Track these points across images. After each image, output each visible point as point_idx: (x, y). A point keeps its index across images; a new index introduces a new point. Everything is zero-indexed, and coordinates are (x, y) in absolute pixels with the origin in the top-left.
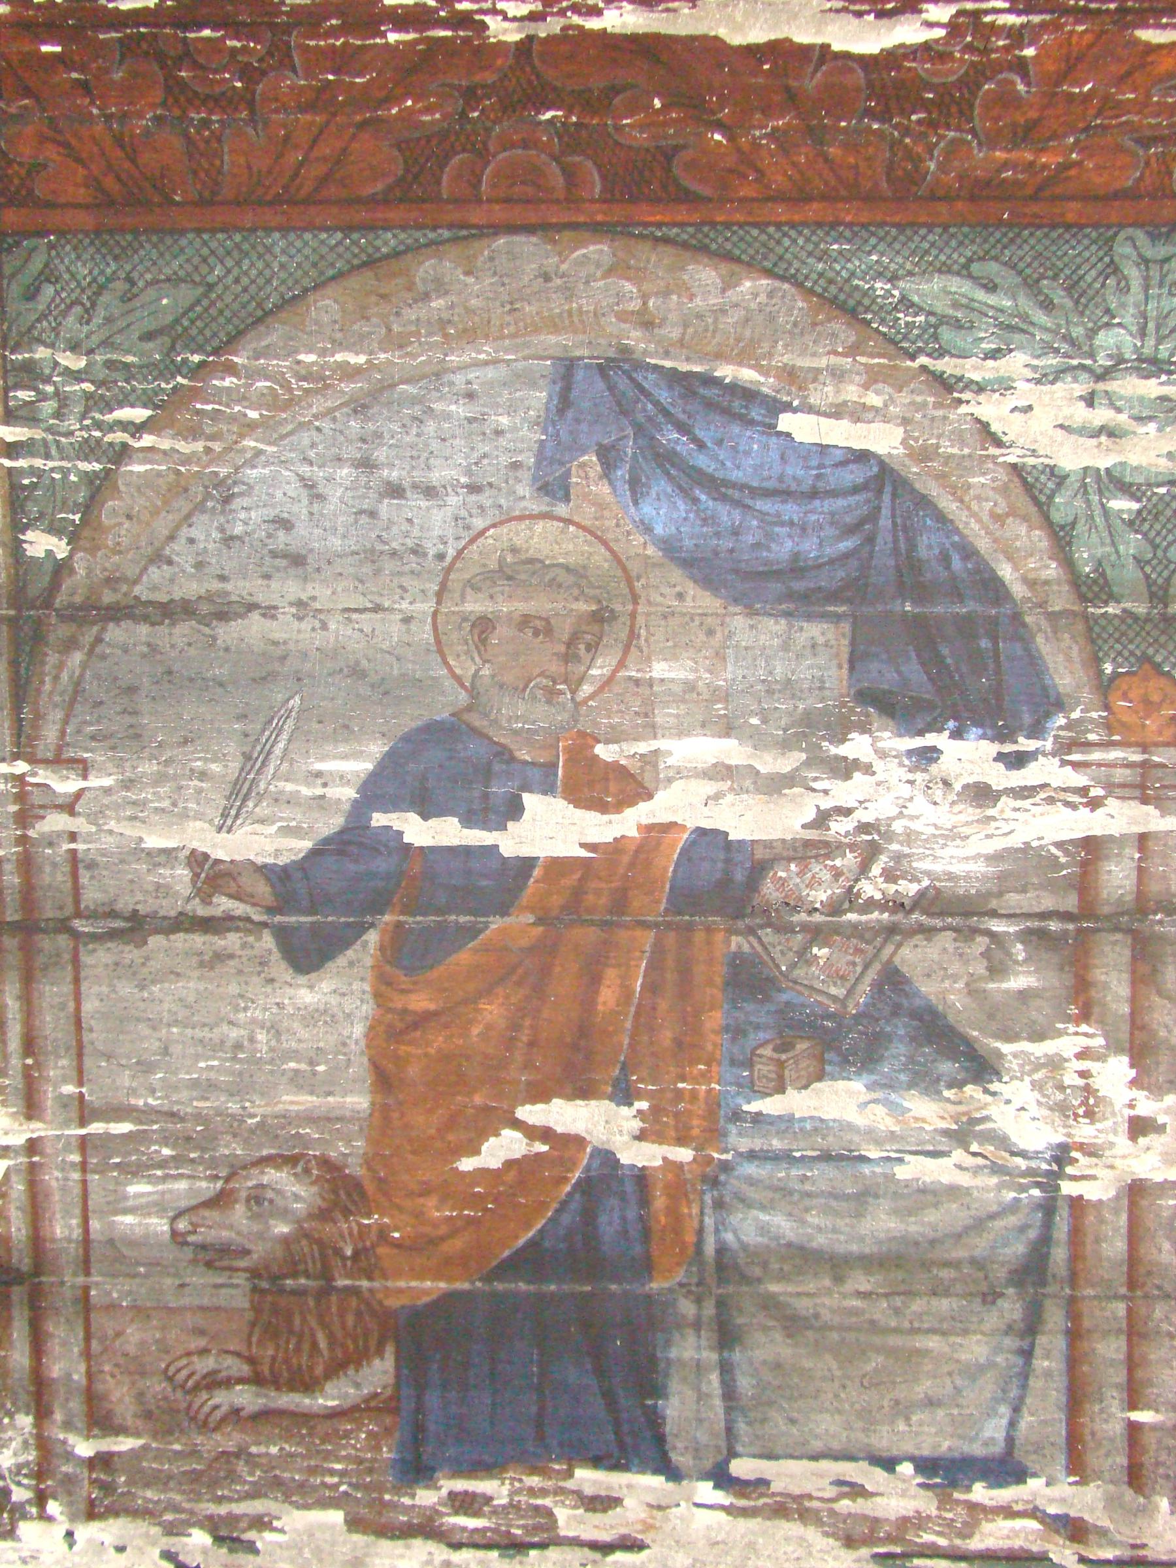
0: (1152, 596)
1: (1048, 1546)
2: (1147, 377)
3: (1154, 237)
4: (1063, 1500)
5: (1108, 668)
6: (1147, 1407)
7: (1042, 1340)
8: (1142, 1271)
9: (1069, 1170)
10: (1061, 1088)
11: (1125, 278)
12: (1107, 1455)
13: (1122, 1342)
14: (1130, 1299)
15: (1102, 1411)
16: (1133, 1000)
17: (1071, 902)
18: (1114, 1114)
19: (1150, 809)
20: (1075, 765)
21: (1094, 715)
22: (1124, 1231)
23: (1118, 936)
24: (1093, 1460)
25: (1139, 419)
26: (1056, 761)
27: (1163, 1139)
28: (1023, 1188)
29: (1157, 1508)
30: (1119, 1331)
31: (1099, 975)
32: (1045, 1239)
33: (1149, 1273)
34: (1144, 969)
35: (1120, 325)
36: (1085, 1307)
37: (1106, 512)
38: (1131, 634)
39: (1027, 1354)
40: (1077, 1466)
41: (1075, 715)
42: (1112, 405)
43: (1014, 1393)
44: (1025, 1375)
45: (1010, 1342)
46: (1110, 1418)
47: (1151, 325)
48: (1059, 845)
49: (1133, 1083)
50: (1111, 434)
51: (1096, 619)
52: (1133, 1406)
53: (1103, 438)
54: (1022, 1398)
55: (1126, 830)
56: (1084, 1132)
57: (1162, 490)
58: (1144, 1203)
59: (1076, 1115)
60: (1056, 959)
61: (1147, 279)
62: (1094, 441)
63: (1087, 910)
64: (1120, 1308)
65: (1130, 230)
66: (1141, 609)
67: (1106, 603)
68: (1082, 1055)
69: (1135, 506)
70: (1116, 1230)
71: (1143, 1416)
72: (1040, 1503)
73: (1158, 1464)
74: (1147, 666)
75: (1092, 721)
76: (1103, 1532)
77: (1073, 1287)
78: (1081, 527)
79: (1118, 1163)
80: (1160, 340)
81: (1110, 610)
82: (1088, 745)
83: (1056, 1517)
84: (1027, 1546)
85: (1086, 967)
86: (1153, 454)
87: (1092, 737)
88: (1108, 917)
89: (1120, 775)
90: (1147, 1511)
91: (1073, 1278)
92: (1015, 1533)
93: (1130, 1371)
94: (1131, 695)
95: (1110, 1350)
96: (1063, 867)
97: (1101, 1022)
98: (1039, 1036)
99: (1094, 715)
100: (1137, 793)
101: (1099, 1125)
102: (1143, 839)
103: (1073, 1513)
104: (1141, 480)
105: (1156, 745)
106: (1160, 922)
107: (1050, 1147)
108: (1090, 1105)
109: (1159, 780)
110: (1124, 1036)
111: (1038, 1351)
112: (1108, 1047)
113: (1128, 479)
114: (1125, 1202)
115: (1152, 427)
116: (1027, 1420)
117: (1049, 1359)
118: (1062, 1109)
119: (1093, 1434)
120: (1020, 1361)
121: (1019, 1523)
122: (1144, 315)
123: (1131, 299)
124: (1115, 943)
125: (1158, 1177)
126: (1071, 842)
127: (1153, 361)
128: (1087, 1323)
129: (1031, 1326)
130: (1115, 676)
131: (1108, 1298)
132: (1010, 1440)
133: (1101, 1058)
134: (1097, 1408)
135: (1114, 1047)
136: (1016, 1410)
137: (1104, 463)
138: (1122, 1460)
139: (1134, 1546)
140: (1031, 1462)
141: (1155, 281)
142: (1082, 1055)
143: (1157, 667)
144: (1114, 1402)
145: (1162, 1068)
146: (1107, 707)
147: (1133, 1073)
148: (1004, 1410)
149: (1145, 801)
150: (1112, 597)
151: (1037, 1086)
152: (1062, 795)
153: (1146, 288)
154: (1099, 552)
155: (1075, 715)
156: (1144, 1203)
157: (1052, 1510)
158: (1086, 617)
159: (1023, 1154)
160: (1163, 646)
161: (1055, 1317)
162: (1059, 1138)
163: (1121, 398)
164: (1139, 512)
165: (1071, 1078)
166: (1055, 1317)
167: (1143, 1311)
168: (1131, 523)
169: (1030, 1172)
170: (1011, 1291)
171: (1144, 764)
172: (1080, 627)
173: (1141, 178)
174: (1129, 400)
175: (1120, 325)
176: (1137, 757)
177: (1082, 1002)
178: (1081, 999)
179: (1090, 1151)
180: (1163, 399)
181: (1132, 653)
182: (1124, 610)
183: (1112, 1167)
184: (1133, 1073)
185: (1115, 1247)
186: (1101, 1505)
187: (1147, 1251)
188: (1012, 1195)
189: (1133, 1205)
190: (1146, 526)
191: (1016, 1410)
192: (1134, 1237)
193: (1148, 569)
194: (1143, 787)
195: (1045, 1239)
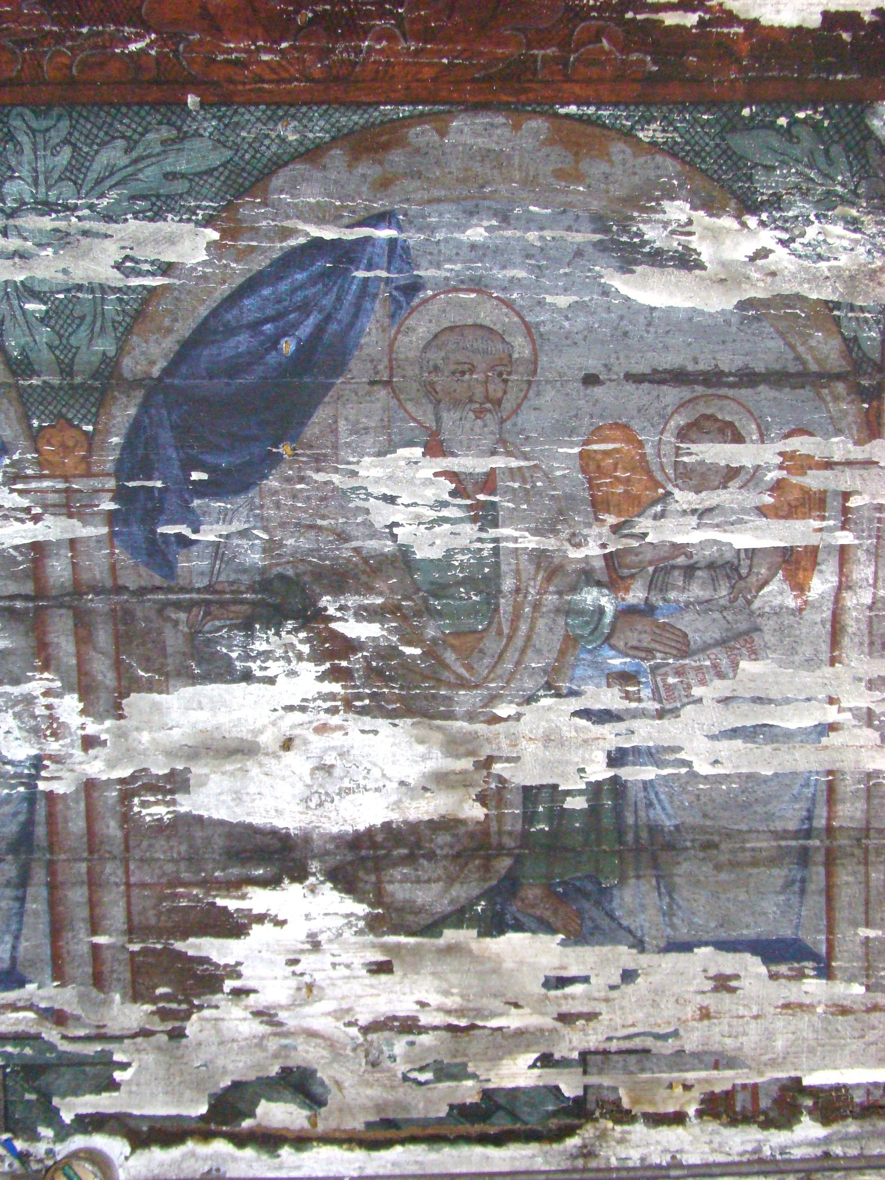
0: (62, 371)
1: (41, 1029)
2: (42, 215)
3: (37, 114)
4: (50, 998)
5: (35, 423)
6: (104, 933)
7: (31, 891)
8: (97, 841)
9: (43, 774)
10: (35, 717)
11: (19, 143)
12: (79, 966)
13: (85, 890)
14: (89, 860)
15: (74, 937)
16: (79, 655)
17: (28, 588)
18: (71, 734)
19: (74, 521)
20: (21, 492)
21: (29, 456)
22: (83, 814)
23: (63, 611)
24: (69, 970)
25: (40, 245)
26: (6, 490)
27: (106, 750)
28: (13, 787)
29: (113, 1001)
30: (83, 882)
31: (52, 638)
32: (30, 823)
33: (102, 843)
34: (83, 632)
35: (19, 178)
36: (60, 867)
37: (24, 312)
38: (49, 399)
39: (22, 900)
40: (59, 974)
41: (16, 457)
42: (20, 235)
43: (14, 927)
44: (21, 913)
45: (9, 892)
46: (80, 941)
47: (41, 178)
48: (16, 548)
49: (83, 712)
50: (22, 257)
51: (25, 388)
52: (94, 932)
53: (17, 260)
54: (20, 930)
55: (59, 536)
56: (53, 746)
57: (61, 296)
58: (96, 795)
59: (46, 736)
60: (22, 628)
61: (34, 144)
62: (10, 262)
63: (40, 593)
64: (83, 867)
65: (19, 109)
66: (56, 381)
67: (31, 377)
68: (47, 693)
69: (44, 308)
70: (78, 813)
71: (102, 940)
72: (35, 1000)
73: (112, 971)
74: (62, 421)
75: (28, 460)
76: (78, 1018)
77: (52, 852)
78: (8, 324)
79: (77, 767)
80: (49, 188)
81: (34, 382)
82: (27, 478)
83: (46, 1010)
84: (27, 1029)
85: (45, 633)
86: (53, 270)
87: (29, 472)
88: (55, 598)
89: (52, 498)
90: (106, 1003)
91: (51, 848)
92: (18, 1021)
93: (92, 909)
94: (53, 441)
95: (77, 895)
96: (21, 563)
97: (57, 671)
98: (16, 681)
99: (29, 456)
100: (64, 510)
101: (61, 742)
102: (73, 543)
103: (57, 1007)
104: (46, 289)
105: (74, 476)
106: (91, 600)
107: (29, 758)
108: (55, 728)
109: (79, 501)
110: (74, 677)
111: (29, 898)
112: (63, 687)
113: (37, 289)
114: (83, 795)
115: (50, 251)
116: (24, 944)
117: (37, 904)
118: (35, 731)
119: (68, 952)
120: (17, 905)
121: (21, 1014)
122: (35, 170)
123: (25, 159)
124: (61, 616)
125: (104, 777)
126: (23, 545)
127: (46, 203)
128: (60, 878)
129: (23, 881)
130: (41, 428)
131: (75, 860)
132: (13, 959)
133: (59, 695)
134: (70, 935)
135: (68, 688)
136: (17, 937)
137: (20, 277)
138: (89, 970)
139: (98, 1027)
140: (28, 973)
141: (41, 146)
142: (47, 693)
143: (69, 422)
144: (82, 928)
145: (102, 702)
146: (37, 451)
147: (81, 706)
148: (8, 938)
149: (70, 516)
150: (34, 373)
151: (16, 715)
152: (13, 513)
153: (35, 151)
154: (23, 341)
155: (16, 457)
156: (96, 795)
157: (43, 1005)
158: (17, 387)
159: (11, 763)
160: (72, 406)
161: (39, 875)
162: (34, 752)
163: (26, 230)
164: (47, 312)
165: (40, 711)
166: (39, 875)
167: (98, 869)
168: (42, 320)
169: (16, 776)
170: (10, 857)
171: (67, 490)
172: (14, 394)
173: (22, 69)
174: (32, 232)
175: (19, 178)
176: (61, 486)
177: (43, 656)
178: (43, 654)
179: (57, 759)
180: (56, 230)
181: (51, 412)
182: (45, 382)
183: (72, 770)
184: (81, 706)
185: (77, 825)
186: (76, 1000)
187: (99, 826)
188: (6, 791)
189: (88, 797)
190: (53, 322)
191: (17, 937)
192: (90, 816)
193: (57, 352)
194: (67, 506)
195: (30, 823)
